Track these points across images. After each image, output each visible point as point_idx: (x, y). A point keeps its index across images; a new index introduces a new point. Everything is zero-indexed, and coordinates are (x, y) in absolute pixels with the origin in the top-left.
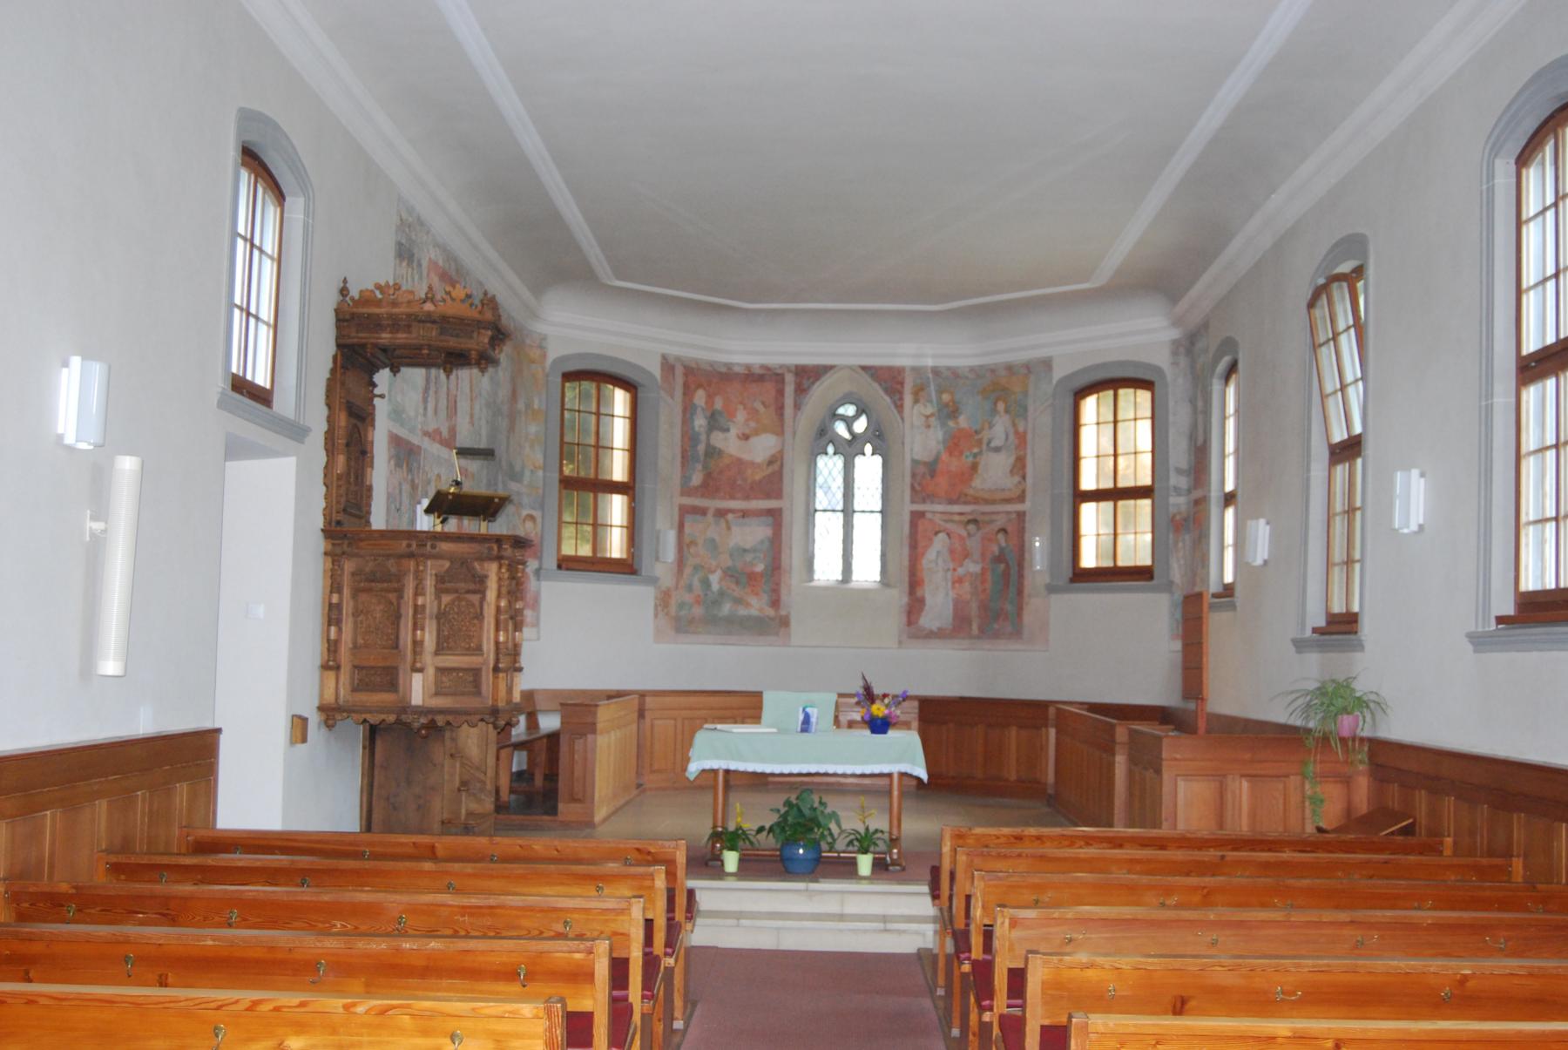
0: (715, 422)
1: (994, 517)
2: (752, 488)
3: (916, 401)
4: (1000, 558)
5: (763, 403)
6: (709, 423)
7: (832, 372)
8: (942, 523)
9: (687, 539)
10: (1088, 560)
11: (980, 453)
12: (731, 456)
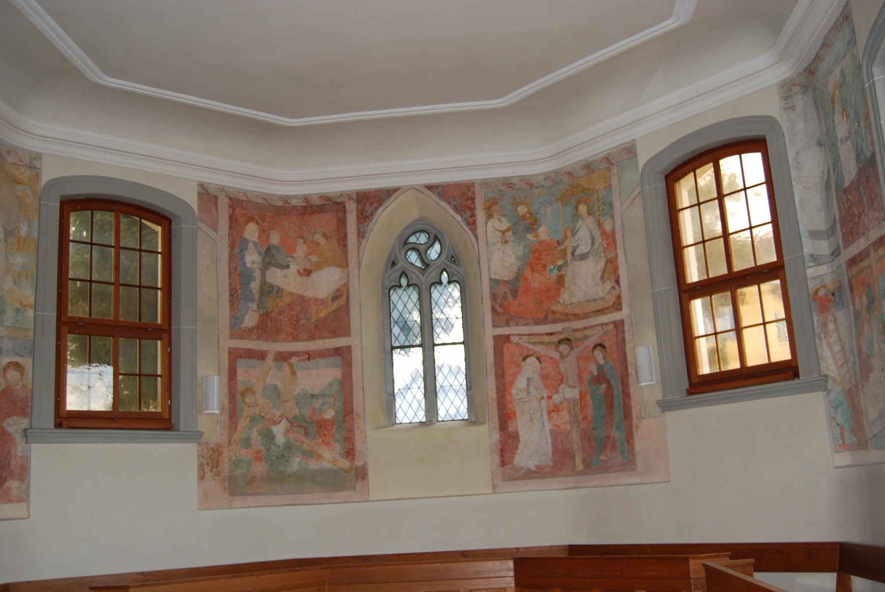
0: (269, 257)
1: (589, 332)
2: (316, 327)
3: (490, 217)
4: (600, 378)
5: (324, 235)
6: (264, 259)
7: (396, 194)
8: (530, 346)
9: (241, 387)
10: (705, 368)
11: (566, 264)
12: (292, 294)
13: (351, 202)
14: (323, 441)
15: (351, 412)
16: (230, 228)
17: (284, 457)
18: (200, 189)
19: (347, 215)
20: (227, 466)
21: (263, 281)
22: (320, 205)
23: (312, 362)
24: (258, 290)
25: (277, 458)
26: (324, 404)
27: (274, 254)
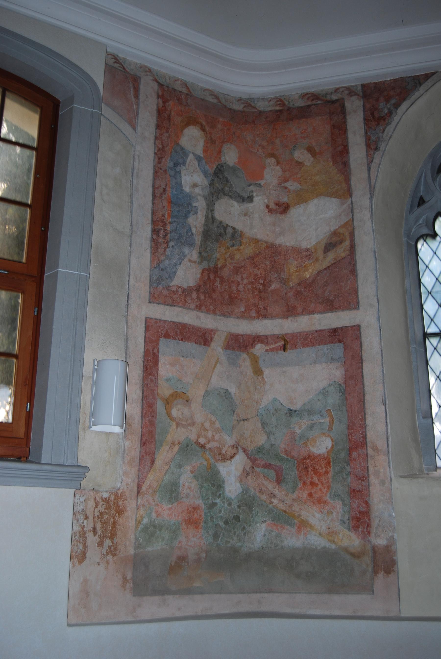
5: (310, 150)
6: (212, 184)
7: (429, 82)
12: (257, 241)
13: (354, 98)
14: (310, 495)
15: (363, 444)
16: (158, 127)
17: (239, 521)
18: (111, 62)
19: (348, 117)
20: (133, 536)
21: (210, 216)
22: (302, 107)
23: (291, 354)
24: (201, 229)
25: (226, 523)
26: (311, 427)
27: (229, 178)
